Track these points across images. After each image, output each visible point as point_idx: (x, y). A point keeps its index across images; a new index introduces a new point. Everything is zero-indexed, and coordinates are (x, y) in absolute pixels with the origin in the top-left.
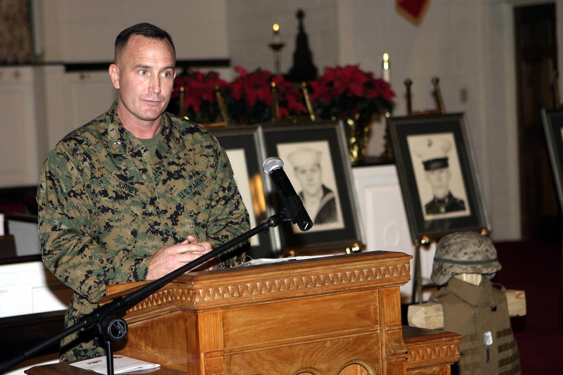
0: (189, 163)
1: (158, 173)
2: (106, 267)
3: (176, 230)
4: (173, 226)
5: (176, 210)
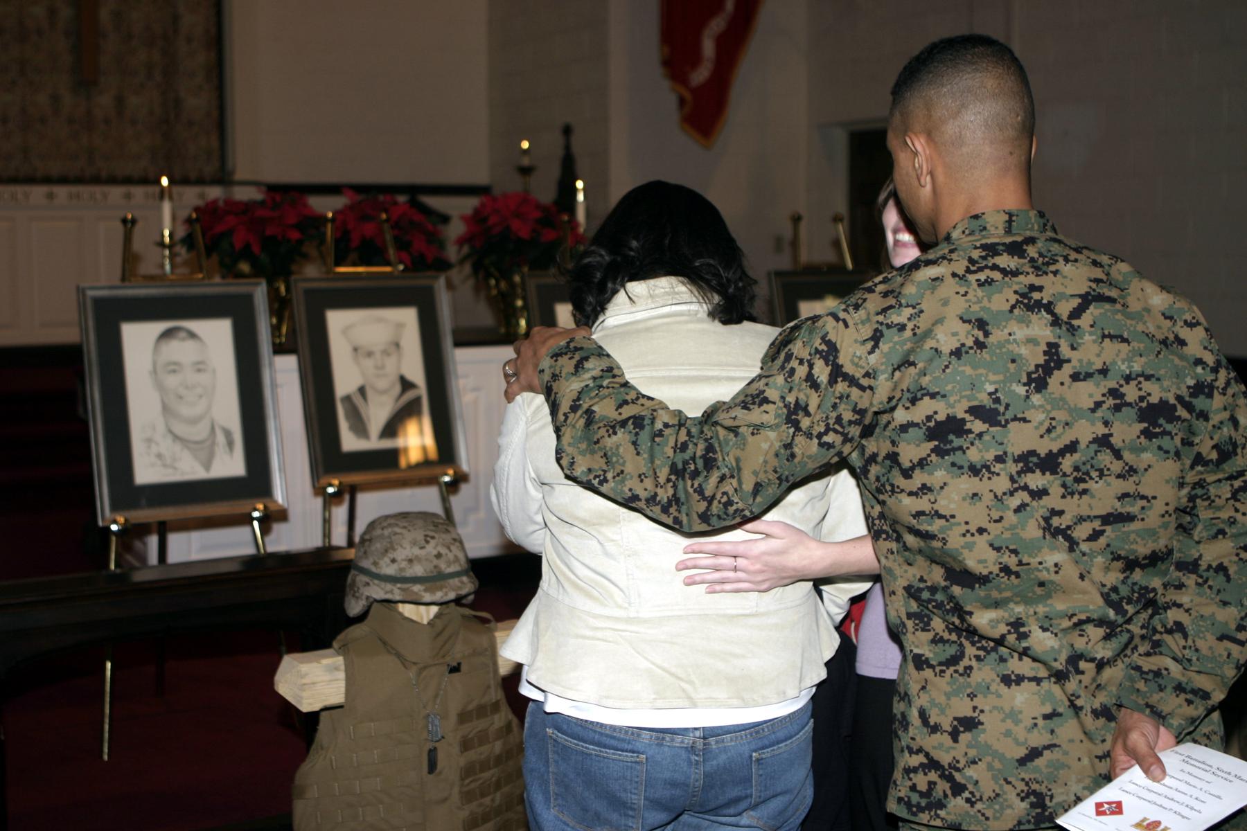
0: (996, 497)
1: (1084, 469)
2: (975, 656)
3: (1051, 331)
4: (1057, 341)
5: (1049, 380)
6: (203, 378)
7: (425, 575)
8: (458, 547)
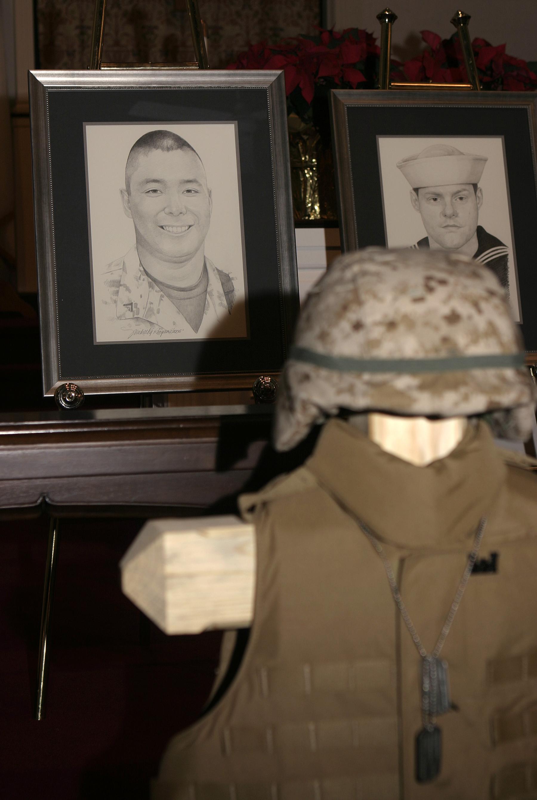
6: (192, 200)
7: (421, 355)
8: (496, 307)
